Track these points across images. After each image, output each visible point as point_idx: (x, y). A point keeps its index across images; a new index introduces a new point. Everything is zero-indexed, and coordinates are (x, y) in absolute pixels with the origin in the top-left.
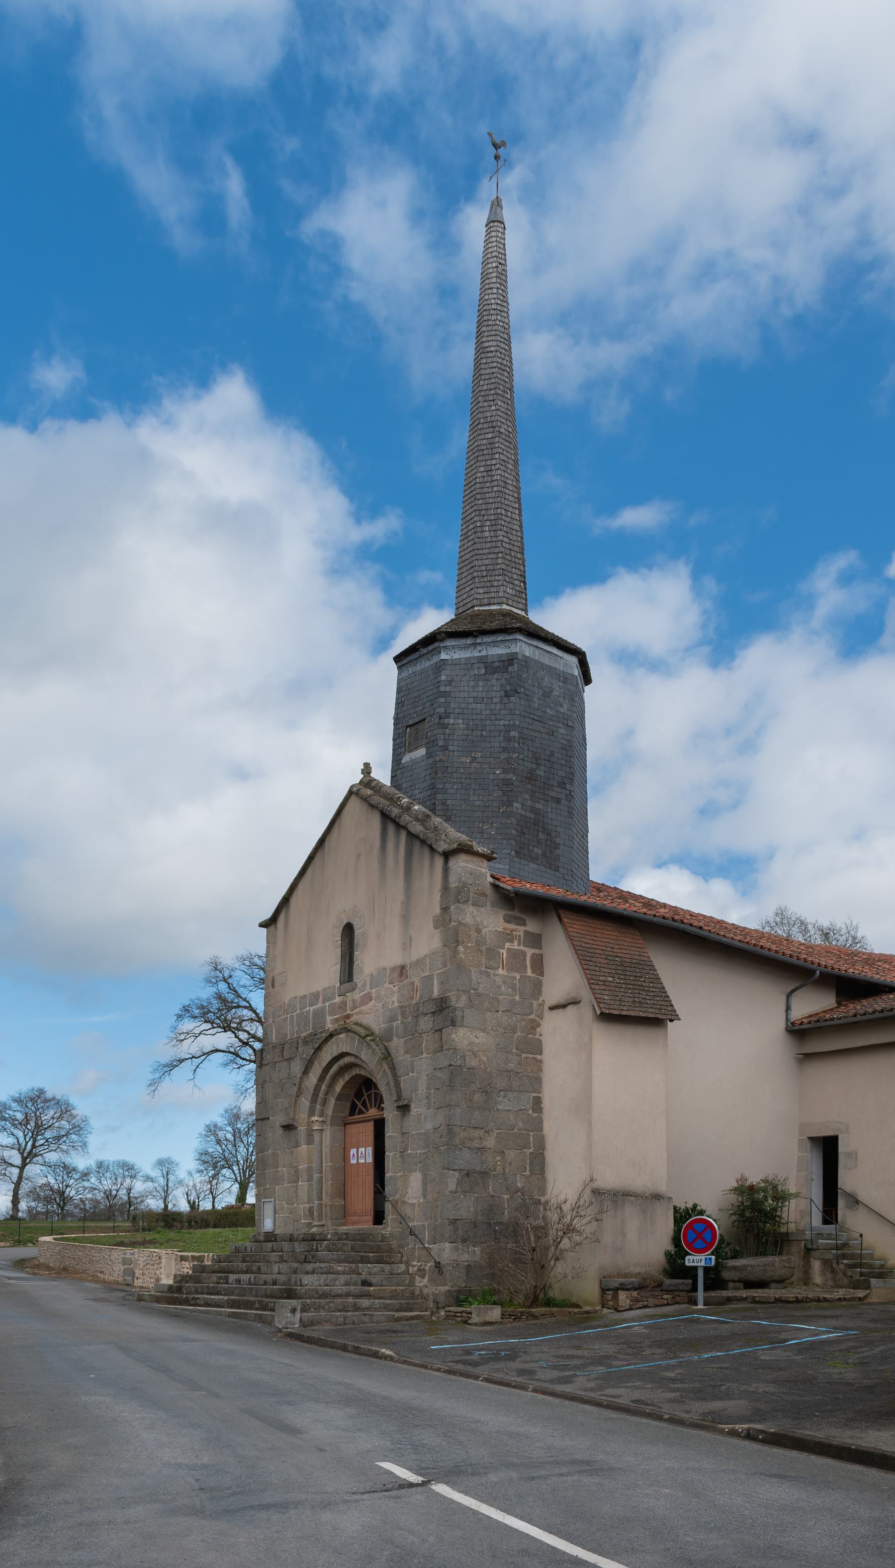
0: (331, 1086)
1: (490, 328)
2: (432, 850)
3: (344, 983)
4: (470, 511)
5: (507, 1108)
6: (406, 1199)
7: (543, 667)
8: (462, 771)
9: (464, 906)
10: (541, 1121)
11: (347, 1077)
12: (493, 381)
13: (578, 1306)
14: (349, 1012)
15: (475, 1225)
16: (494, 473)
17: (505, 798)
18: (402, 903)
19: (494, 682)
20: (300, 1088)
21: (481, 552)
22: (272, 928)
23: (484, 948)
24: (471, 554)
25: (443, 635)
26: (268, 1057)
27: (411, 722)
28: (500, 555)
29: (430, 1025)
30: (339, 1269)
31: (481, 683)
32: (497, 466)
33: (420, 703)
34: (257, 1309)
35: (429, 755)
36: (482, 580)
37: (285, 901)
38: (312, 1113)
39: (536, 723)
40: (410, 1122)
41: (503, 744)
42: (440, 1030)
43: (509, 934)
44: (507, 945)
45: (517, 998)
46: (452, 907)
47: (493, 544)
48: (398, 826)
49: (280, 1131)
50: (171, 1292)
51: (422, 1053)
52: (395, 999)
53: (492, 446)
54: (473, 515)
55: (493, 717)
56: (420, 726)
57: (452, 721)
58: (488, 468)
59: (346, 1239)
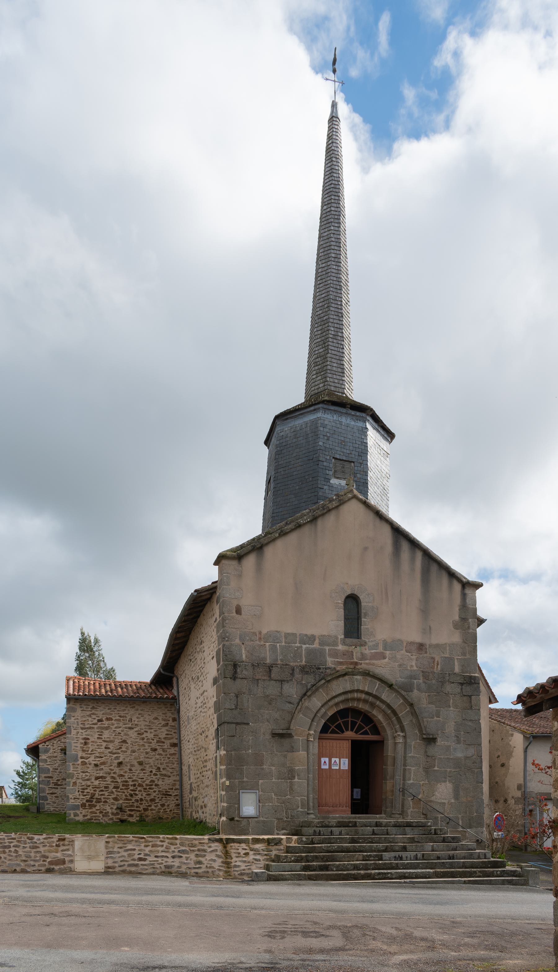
6: (433, 798)
14: (355, 660)
27: (338, 457)
40: (433, 750)
42: (470, 696)
46: (470, 620)
49: (268, 736)
51: (450, 707)
52: (414, 664)
56: (347, 465)
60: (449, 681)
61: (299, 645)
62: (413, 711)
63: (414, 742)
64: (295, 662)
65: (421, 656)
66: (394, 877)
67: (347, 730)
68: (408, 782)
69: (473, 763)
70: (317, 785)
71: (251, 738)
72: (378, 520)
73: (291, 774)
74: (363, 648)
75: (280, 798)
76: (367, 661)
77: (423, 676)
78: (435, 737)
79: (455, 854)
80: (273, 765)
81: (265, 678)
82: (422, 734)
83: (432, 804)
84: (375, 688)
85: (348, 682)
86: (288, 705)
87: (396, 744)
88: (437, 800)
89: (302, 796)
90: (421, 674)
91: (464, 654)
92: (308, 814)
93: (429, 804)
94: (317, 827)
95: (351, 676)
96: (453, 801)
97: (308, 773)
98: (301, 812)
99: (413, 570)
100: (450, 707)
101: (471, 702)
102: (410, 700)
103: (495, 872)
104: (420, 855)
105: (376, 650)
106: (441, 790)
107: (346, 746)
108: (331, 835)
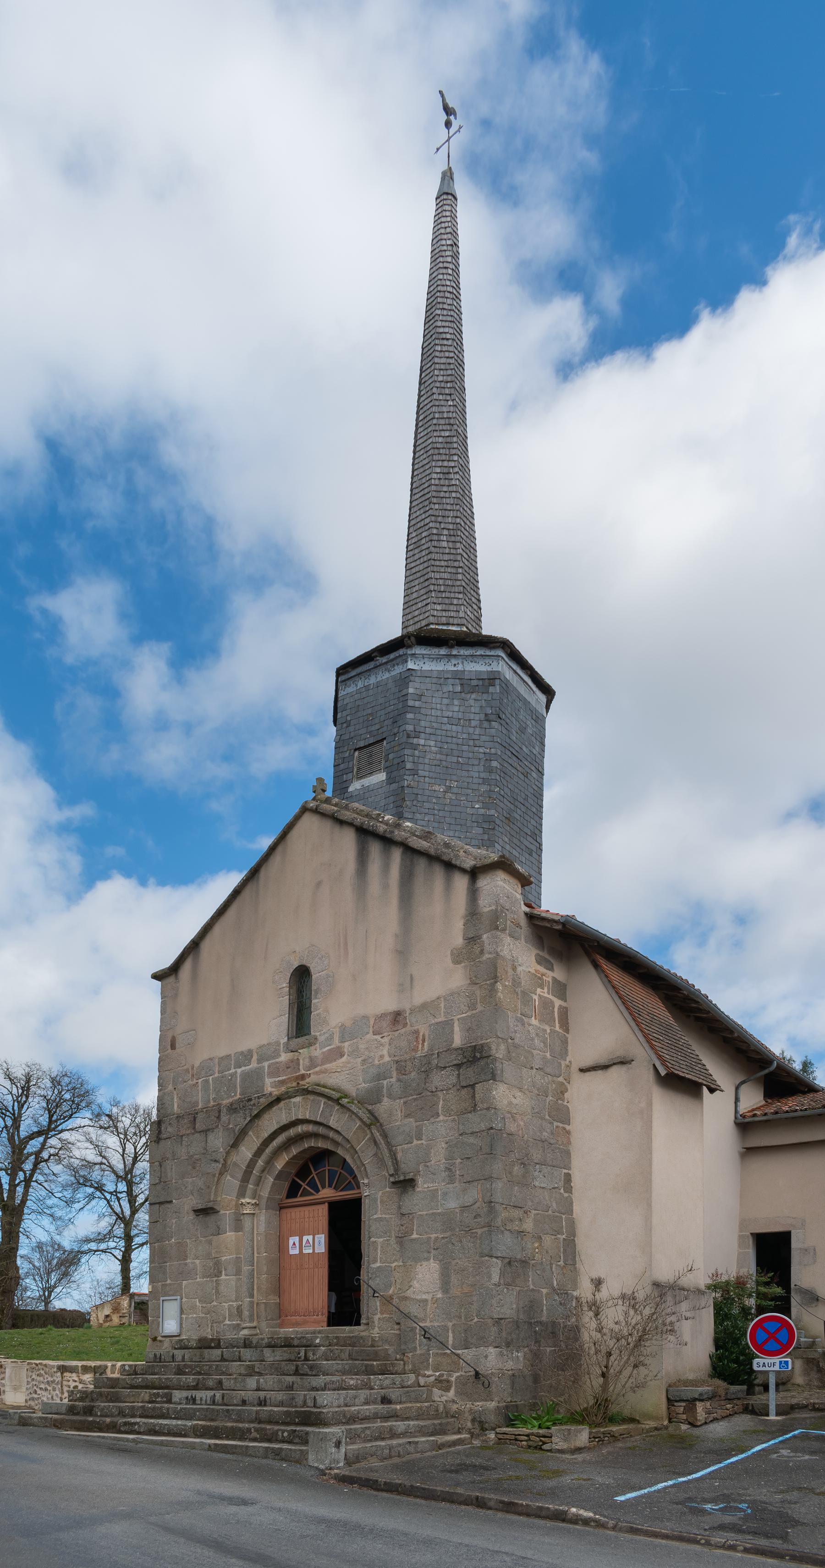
0: (270, 1162)
1: (445, 312)
2: (450, 866)
3: (292, 1038)
4: (423, 516)
5: (542, 1185)
6: (409, 1293)
7: (520, 697)
8: (434, 800)
9: (503, 935)
10: (571, 1204)
11: (294, 1151)
12: (449, 372)
13: (632, 1420)
14: (302, 1072)
15: (517, 1324)
16: (452, 476)
17: (486, 837)
18: (397, 936)
19: (472, 702)
20: (224, 1165)
21: (438, 563)
22: (171, 980)
23: (519, 990)
24: (426, 565)
25: (413, 639)
26: (170, 1129)
27: (362, 744)
28: (460, 570)
29: (453, 1079)
30: (352, 1382)
31: (456, 702)
32: (456, 470)
33: (377, 721)
34: (255, 1440)
35: (390, 780)
36: (439, 595)
37: (194, 946)
38: (242, 1193)
39: (515, 758)
40: (416, 1202)
41: (483, 775)
42: (473, 1086)
43: (539, 978)
44: (539, 990)
45: (548, 1055)
46: (485, 936)
47: (452, 557)
48: (387, 841)
49: (192, 1216)
50: (74, 1414)
51: (438, 1115)
53: (449, 446)
54: (427, 521)
55: (471, 743)
56: (375, 749)
57: (422, 742)
58: (446, 470)
59: (337, 1344)
60: (437, 1067)
64: (228, 1098)
67: (324, 1187)
69: (475, 1217)
71: (174, 1221)
72: (337, 828)
74: (312, 1048)
76: (317, 1069)
77: (397, 1069)
79: (268, 1397)
80: (197, 1258)
81: (189, 1132)
90: (394, 1067)
91: (472, 1006)
95: (287, 1101)
96: (440, 1295)
98: (229, 1325)
99: (385, 886)
101: (474, 1096)
103: (280, 1433)
105: (330, 1045)
107: (322, 1214)
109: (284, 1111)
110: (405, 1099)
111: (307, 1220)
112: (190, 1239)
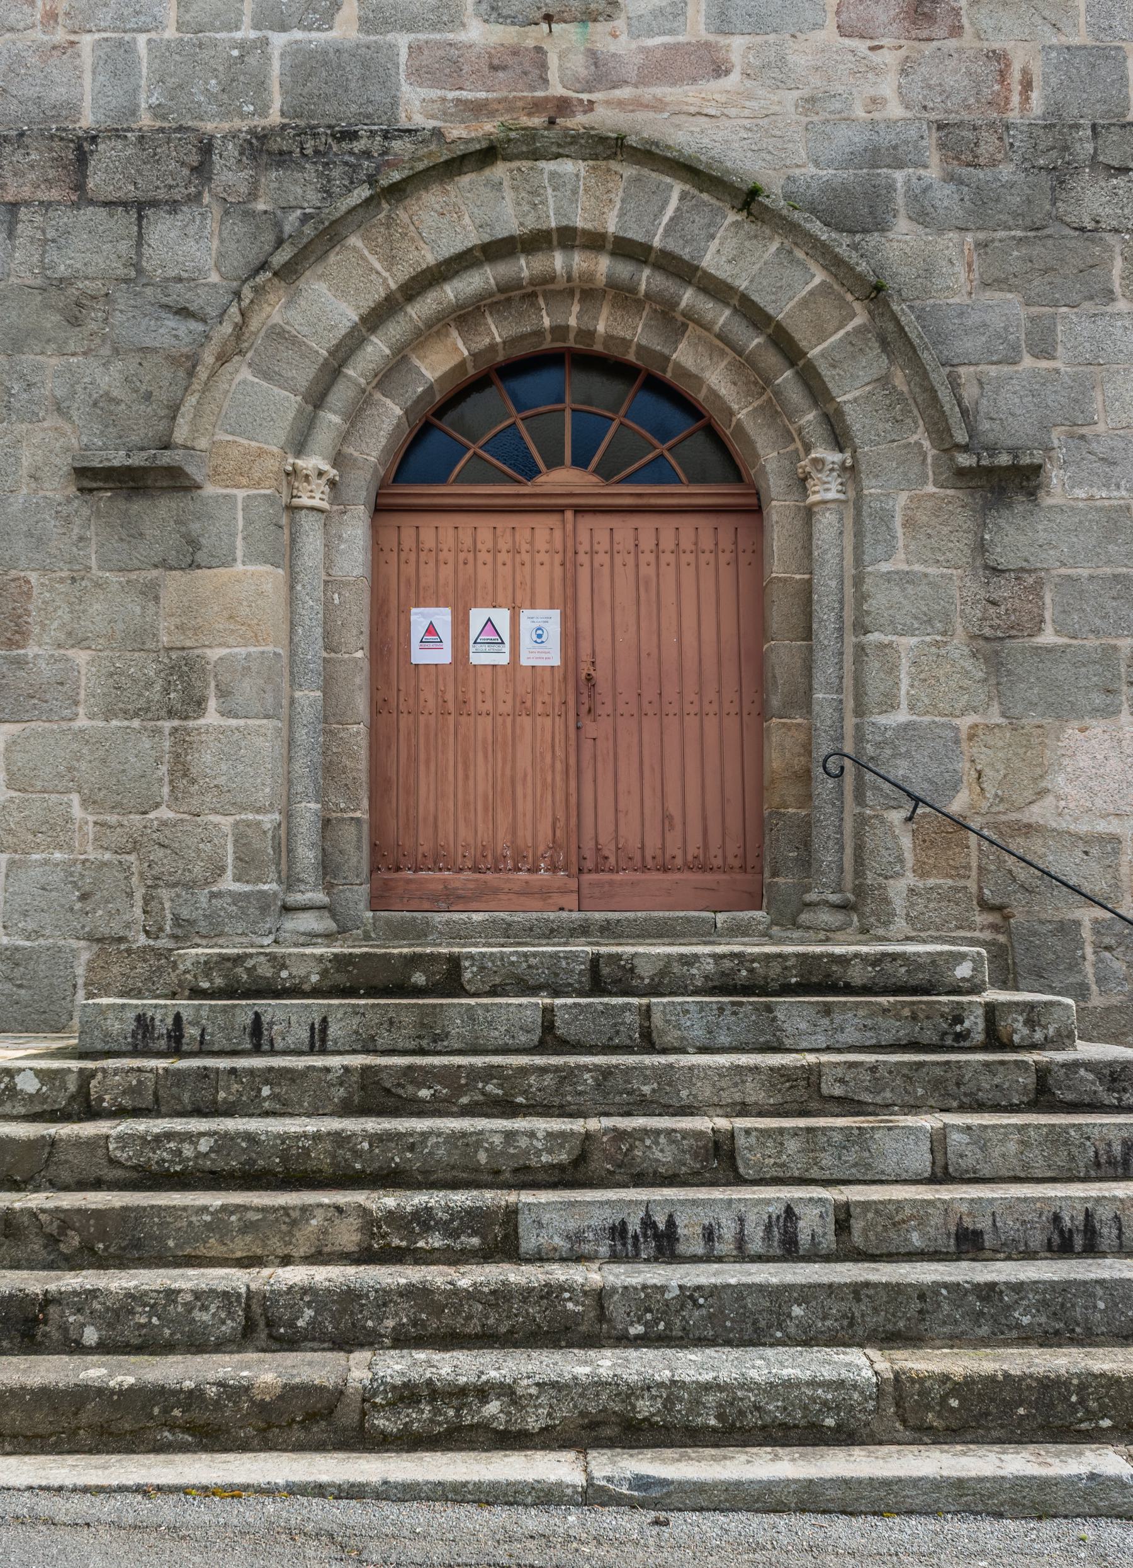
6: (1039, 813)
14: (557, 89)
40: (1016, 536)
49: (58, 488)
51: (1109, 295)
52: (887, 88)
61: (253, 34)
62: (891, 326)
63: (908, 492)
64: (226, 115)
65: (928, 48)
66: (533, 1424)
67: (554, 462)
68: (882, 720)
70: (364, 753)
73: (182, 688)
74: (600, 28)
75: (113, 819)
76: (624, 93)
77: (942, 146)
78: (1026, 460)
79: (1104, 1213)
80: (80, 642)
81: (54, 194)
82: (948, 447)
83: (1035, 847)
84: (663, 213)
85: (509, 195)
86: (171, 322)
87: (808, 514)
88: (1063, 824)
89: (243, 809)
90: (932, 139)
92: (287, 909)
93: (1018, 844)
94: (197, 993)
95: (525, 165)
97: (294, 683)
98: (236, 897)
100: (1109, 295)
102: (862, 267)
104: (812, 1224)
105: (672, 32)
106: (1083, 761)
108: (257, 1051)
109: (509, 195)
110: (981, 236)
111: (483, 556)
112: (44, 569)
